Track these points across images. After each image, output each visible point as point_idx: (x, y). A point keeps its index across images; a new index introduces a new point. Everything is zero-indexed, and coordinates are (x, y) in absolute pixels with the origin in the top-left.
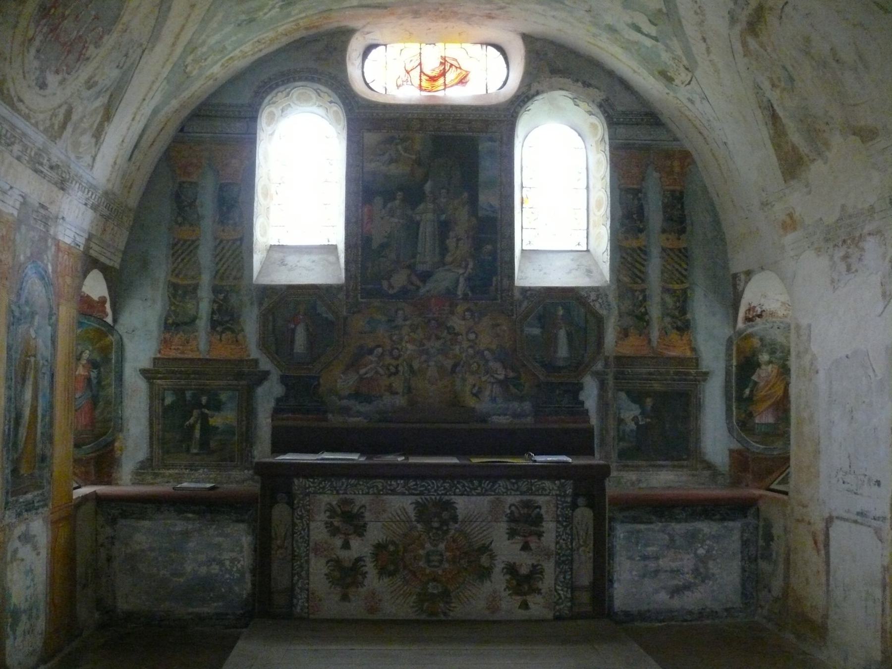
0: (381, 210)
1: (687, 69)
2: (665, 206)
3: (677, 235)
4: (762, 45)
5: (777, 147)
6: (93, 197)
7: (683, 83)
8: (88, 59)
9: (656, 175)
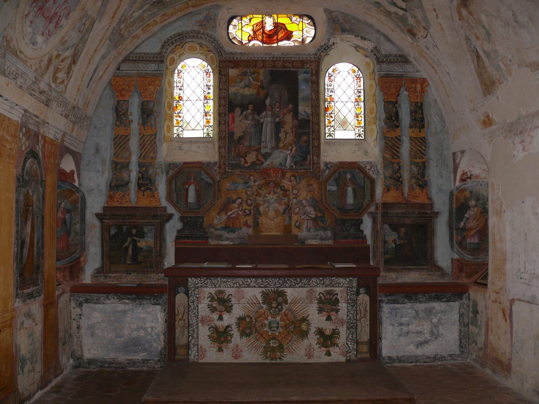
1: (425, 28)
2: (412, 112)
4: (470, 13)
5: (480, 75)
6: (66, 110)
7: (422, 37)
8: (61, 26)
9: (406, 93)
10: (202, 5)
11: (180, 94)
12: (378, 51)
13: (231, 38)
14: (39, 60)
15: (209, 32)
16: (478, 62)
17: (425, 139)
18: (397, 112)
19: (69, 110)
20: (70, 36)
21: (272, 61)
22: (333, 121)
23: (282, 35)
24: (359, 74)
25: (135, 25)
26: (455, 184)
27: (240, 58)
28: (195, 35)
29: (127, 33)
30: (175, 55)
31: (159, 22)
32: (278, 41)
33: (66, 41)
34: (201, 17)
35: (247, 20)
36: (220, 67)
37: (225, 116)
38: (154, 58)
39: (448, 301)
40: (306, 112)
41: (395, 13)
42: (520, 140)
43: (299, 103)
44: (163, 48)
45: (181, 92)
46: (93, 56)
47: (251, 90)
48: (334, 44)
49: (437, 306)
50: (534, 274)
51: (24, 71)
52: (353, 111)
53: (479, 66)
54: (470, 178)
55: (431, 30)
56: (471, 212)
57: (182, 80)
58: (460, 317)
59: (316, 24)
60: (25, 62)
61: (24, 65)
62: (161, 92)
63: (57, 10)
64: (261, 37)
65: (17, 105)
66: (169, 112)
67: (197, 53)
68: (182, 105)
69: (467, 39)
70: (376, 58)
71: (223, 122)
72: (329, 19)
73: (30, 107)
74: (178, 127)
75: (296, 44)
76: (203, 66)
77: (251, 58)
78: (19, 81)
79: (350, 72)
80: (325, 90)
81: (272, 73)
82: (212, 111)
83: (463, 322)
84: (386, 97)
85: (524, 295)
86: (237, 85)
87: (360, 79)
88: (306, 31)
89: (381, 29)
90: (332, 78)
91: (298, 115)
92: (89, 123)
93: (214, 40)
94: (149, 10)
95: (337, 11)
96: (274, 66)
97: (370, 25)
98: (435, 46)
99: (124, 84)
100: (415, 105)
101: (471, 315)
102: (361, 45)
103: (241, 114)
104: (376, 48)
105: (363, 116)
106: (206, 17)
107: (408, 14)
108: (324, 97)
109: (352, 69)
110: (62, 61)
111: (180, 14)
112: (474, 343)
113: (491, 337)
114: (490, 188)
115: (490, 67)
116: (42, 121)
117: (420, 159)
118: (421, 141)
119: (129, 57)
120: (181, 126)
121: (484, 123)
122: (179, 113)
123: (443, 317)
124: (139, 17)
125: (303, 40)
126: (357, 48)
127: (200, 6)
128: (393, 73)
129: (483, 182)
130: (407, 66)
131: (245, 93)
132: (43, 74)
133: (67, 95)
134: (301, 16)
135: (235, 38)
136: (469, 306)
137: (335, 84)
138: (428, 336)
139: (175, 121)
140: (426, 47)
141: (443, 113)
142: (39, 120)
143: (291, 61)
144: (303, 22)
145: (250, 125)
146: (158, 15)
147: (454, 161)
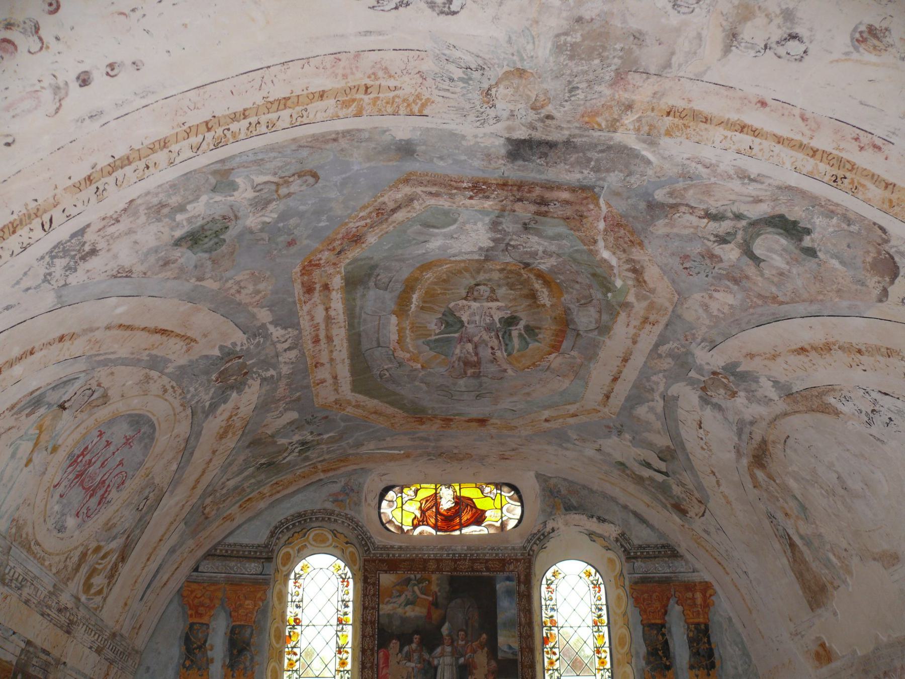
0: (397, 654)
1: (700, 502)
2: (691, 641)
3: (706, 670)
4: (771, 477)
5: (800, 576)
6: (99, 640)
7: (696, 515)
8: (109, 502)
9: (678, 608)
10: (339, 468)
11: (297, 615)
12: (628, 540)
13: (384, 521)
14: (66, 555)
15: (347, 511)
16: (793, 552)
18: (666, 643)
19: (105, 640)
20: (121, 517)
21: (452, 560)
22: (556, 660)
23: (469, 517)
24: (597, 578)
25: (230, 499)
27: (400, 556)
28: (325, 516)
29: (214, 512)
30: (292, 548)
31: (267, 495)
32: (462, 526)
33: (114, 525)
34: (337, 488)
35: (412, 493)
36: (366, 570)
37: (373, 655)
38: (256, 552)
40: (510, 647)
41: (651, 479)
43: (499, 631)
44: (272, 536)
45: (299, 611)
46: (155, 549)
47: (417, 609)
48: (553, 530)
51: (37, 575)
52: (590, 642)
53: (795, 561)
55: (711, 505)
57: (300, 591)
59: (524, 498)
60: (41, 560)
61: (39, 565)
62: (264, 612)
63: (106, 477)
64: (433, 521)
65: (14, 633)
66: (278, 646)
67: (328, 546)
68: (300, 633)
69: (771, 517)
70: (624, 551)
71: (368, 665)
72: (543, 490)
73: (38, 635)
74: (290, 672)
75: (492, 531)
76: (337, 567)
77: (417, 555)
78: (26, 591)
79: (583, 575)
80: (541, 607)
81: (452, 580)
82: (350, 645)
84: (645, 617)
86: (394, 600)
87: (599, 587)
88: (508, 510)
89: (628, 504)
90: (553, 586)
91: (497, 652)
92: (137, 661)
93: (356, 525)
94: (252, 476)
95: (556, 477)
96: (455, 570)
97: (612, 497)
98: (720, 529)
99: (203, 595)
100: (696, 628)
102: (599, 531)
103: (401, 651)
104: (623, 534)
105: (608, 650)
106: (344, 487)
107: (671, 481)
108: (540, 618)
109: (585, 571)
110: (103, 557)
111: (302, 483)
115: (814, 561)
116: (55, 660)
119: (216, 550)
120: (296, 671)
121: (818, 656)
122: (294, 647)
124: (236, 488)
125: (503, 525)
126: (591, 535)
127: (334, 469)
128: (654, 575)
130: (676, 564)
131: (407, 614)
132: (68, 579)
133: (105, 614)
134: (498, 486)
135: (390, 522)
137: (558, 596)
139: (286, 661)
140: (705, 531)
141: (745, 639)
142: (50, 659)
143: (484, 559)
144: (501, 495)
145: (415, 670)
146: (266, 484)
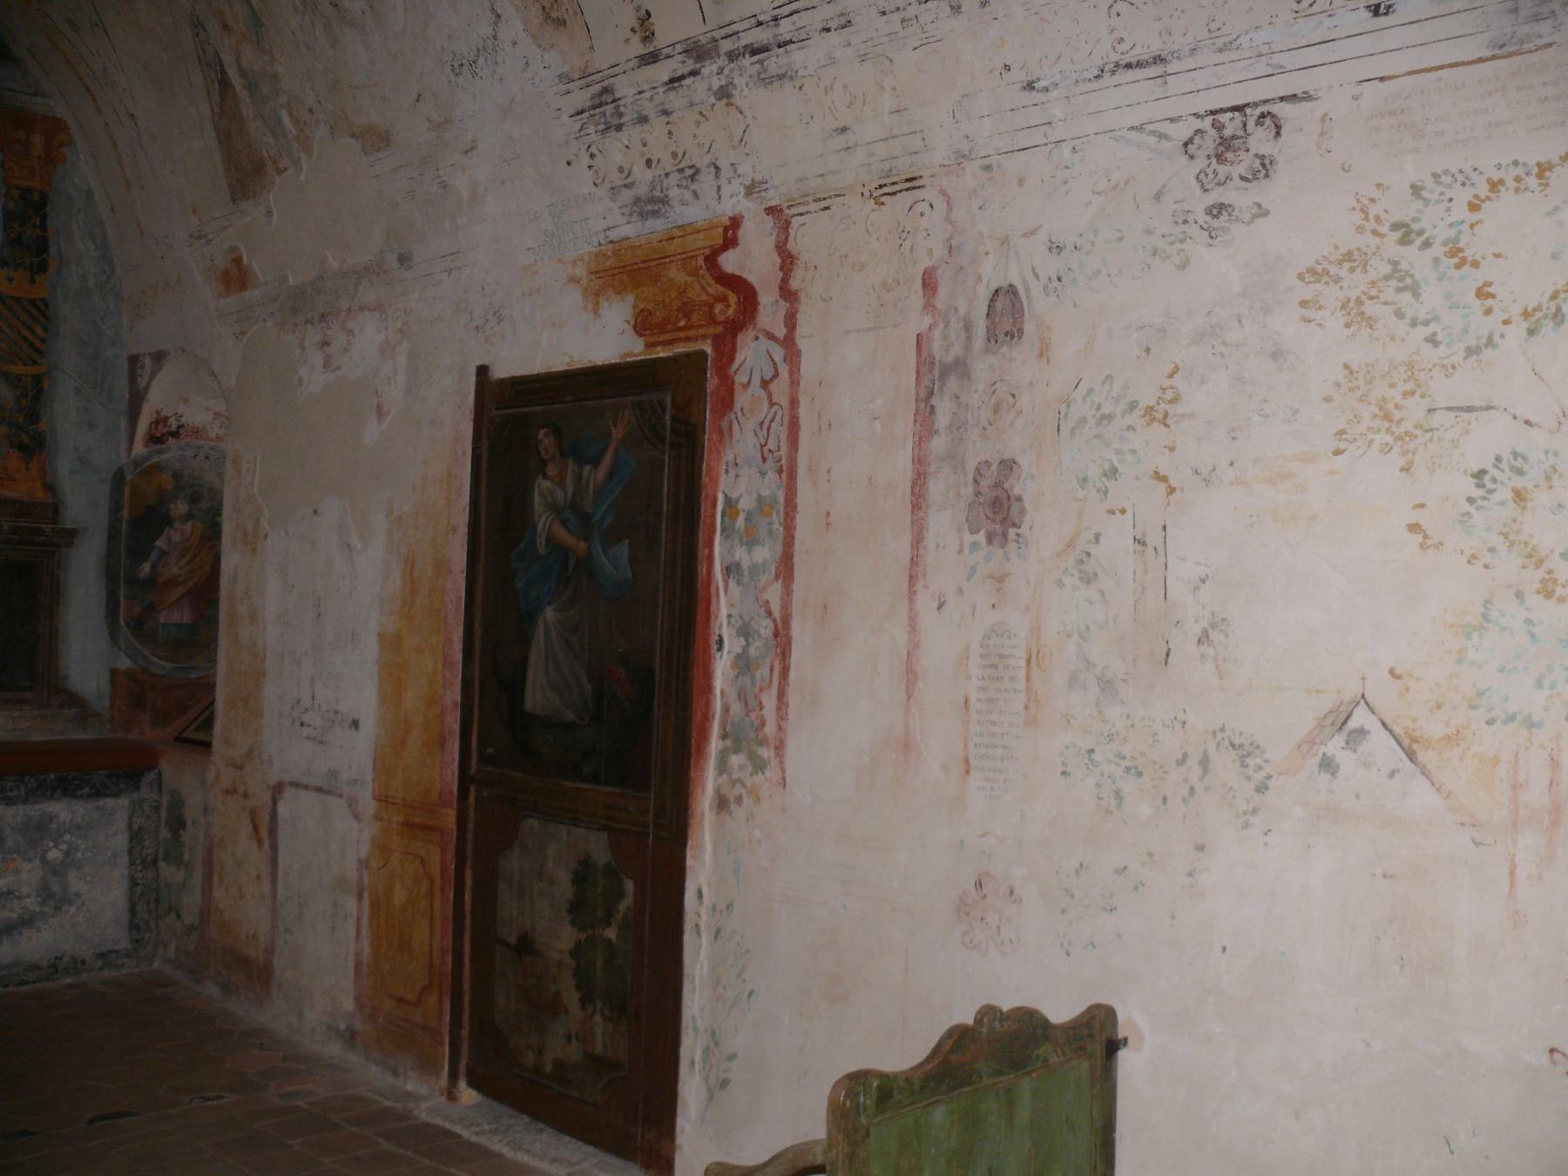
16: (223, 97)
17: (46, 305)
26: (130, 451)
39: (98, 794)
42: (318, 338)
49: (62, 810)
50: (337, 712)
54: (176, 434)
56: (174, 536)
58: (131, 839)
83: (141, 854)
85: (309, 770)
101: (165, 833)
112: (173, 915)
113: (219, 893)
114: (229, 470)
115: (254, 119)
117: (25, 364)
118: (34, 311)
123: (80, 842)
129: (213, 448)
136: (157, 809)
138: (32, 903)
147: (133, 379)
